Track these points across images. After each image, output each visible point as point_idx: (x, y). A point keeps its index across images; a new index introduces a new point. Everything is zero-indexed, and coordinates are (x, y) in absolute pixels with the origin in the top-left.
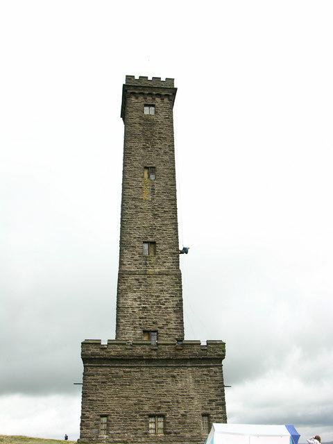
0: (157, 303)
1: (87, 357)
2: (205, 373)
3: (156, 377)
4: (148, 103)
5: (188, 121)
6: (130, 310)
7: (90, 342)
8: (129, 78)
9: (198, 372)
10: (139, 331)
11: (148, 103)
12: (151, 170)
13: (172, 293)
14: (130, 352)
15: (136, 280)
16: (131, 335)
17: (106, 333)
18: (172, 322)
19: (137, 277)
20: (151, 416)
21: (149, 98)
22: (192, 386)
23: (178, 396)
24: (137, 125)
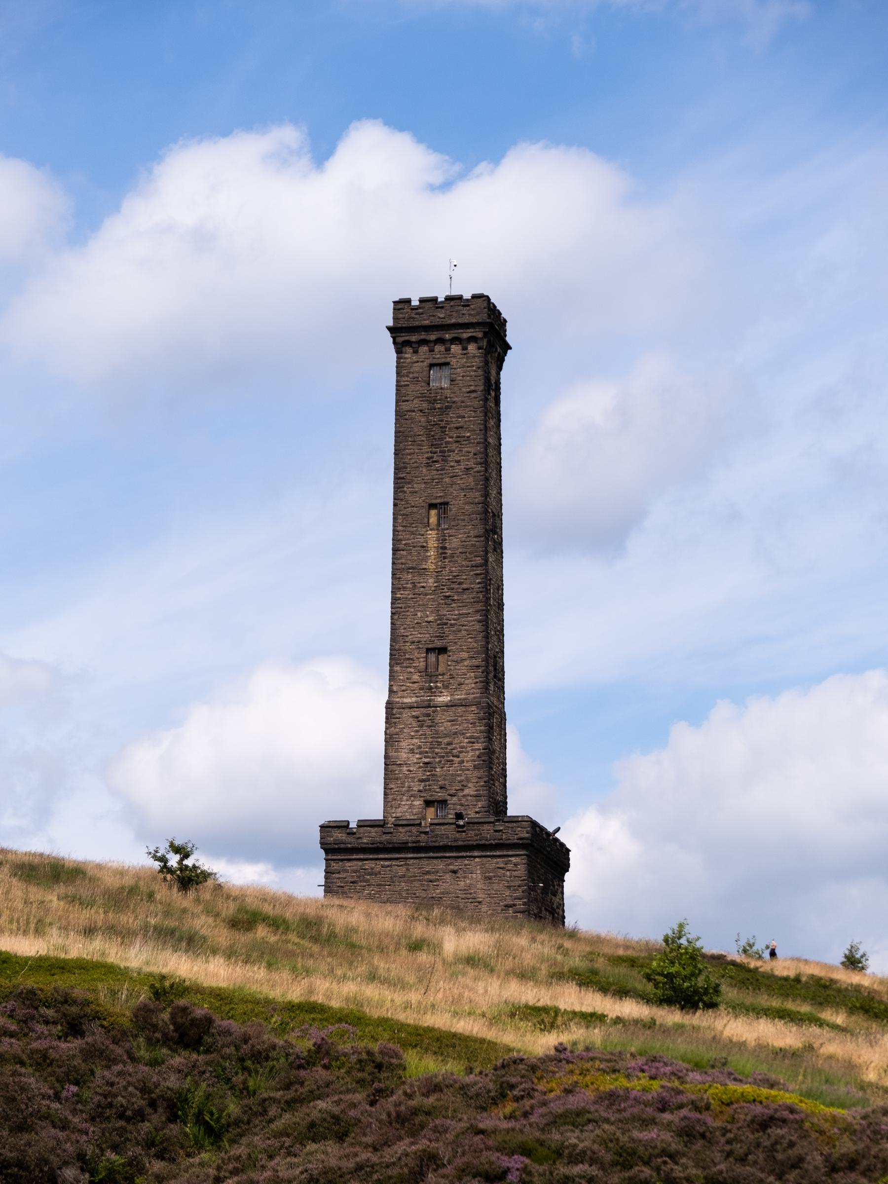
1: (329, 846)
3: (428, 873)
5: (550, 437)
7: (331, 824)
8: (401, 305)
9: (492, 863)
10: (418, 803)
13: (471, 737)
14: (388, 837)
15: (413, 717)
16: (410, 808)
17: (365, 802)
18: (470, 785)
21: (439, 348)
23: (459, 900)
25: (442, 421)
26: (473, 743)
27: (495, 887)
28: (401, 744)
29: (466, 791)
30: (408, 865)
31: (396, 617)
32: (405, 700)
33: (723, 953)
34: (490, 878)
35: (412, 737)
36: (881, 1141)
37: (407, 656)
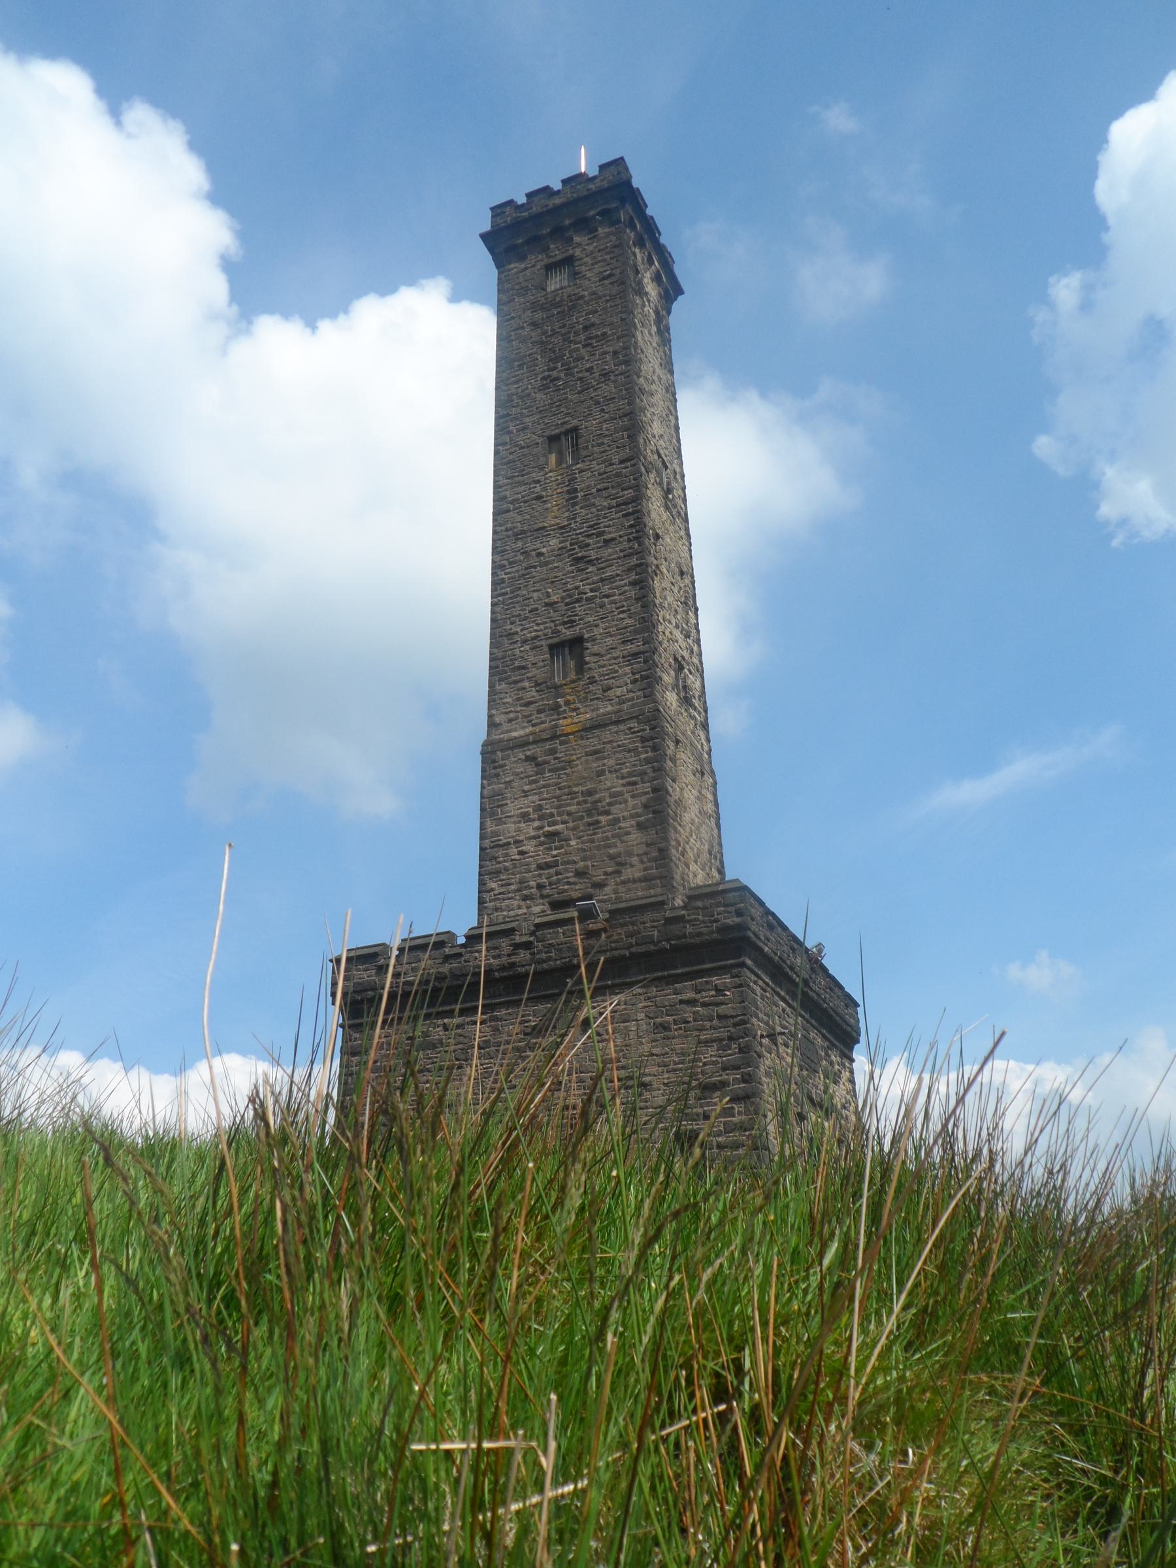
2: (689, 995)
4: (1003, 1034)
6: (513, 851)
9: (668, 995)
11: (1003, 1034)
13: (630, 775)
25: (564, 326)
26: (635, 783)
27: (678, 1044)
28: (506, 809)
29: (628, 873)
30: (497, 1019)
31: (498, 609)
32: (515, 734)
33: (1111, 221)
34: (665, 1027)
35: (526, 794)
36: (529, 1414)
37: (517, 663)
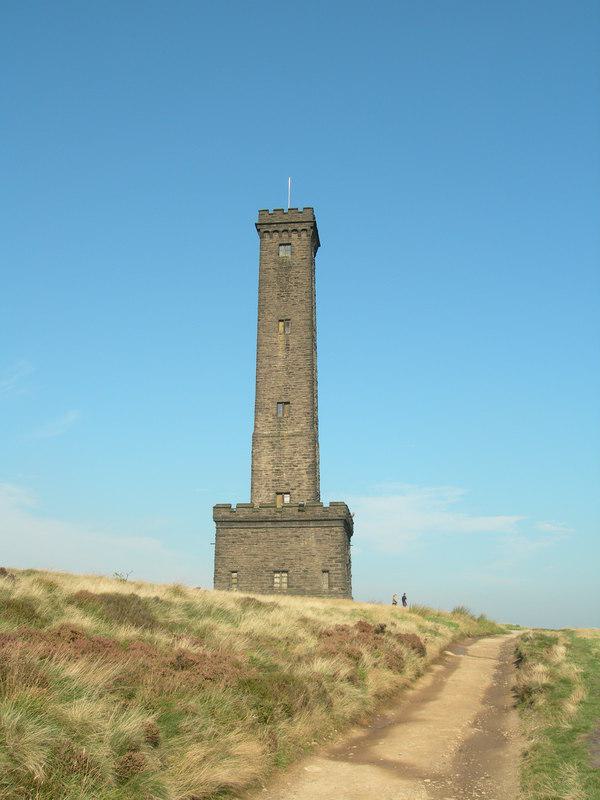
0: (290, 465)
9: (321, 532)
12: (286, 321)
16: (265, 496)
17: (238, 493)
19: (271, 439)
20: (276, 572)
21: (285, 235)
22: (314, 545)
24: (272, 271)
